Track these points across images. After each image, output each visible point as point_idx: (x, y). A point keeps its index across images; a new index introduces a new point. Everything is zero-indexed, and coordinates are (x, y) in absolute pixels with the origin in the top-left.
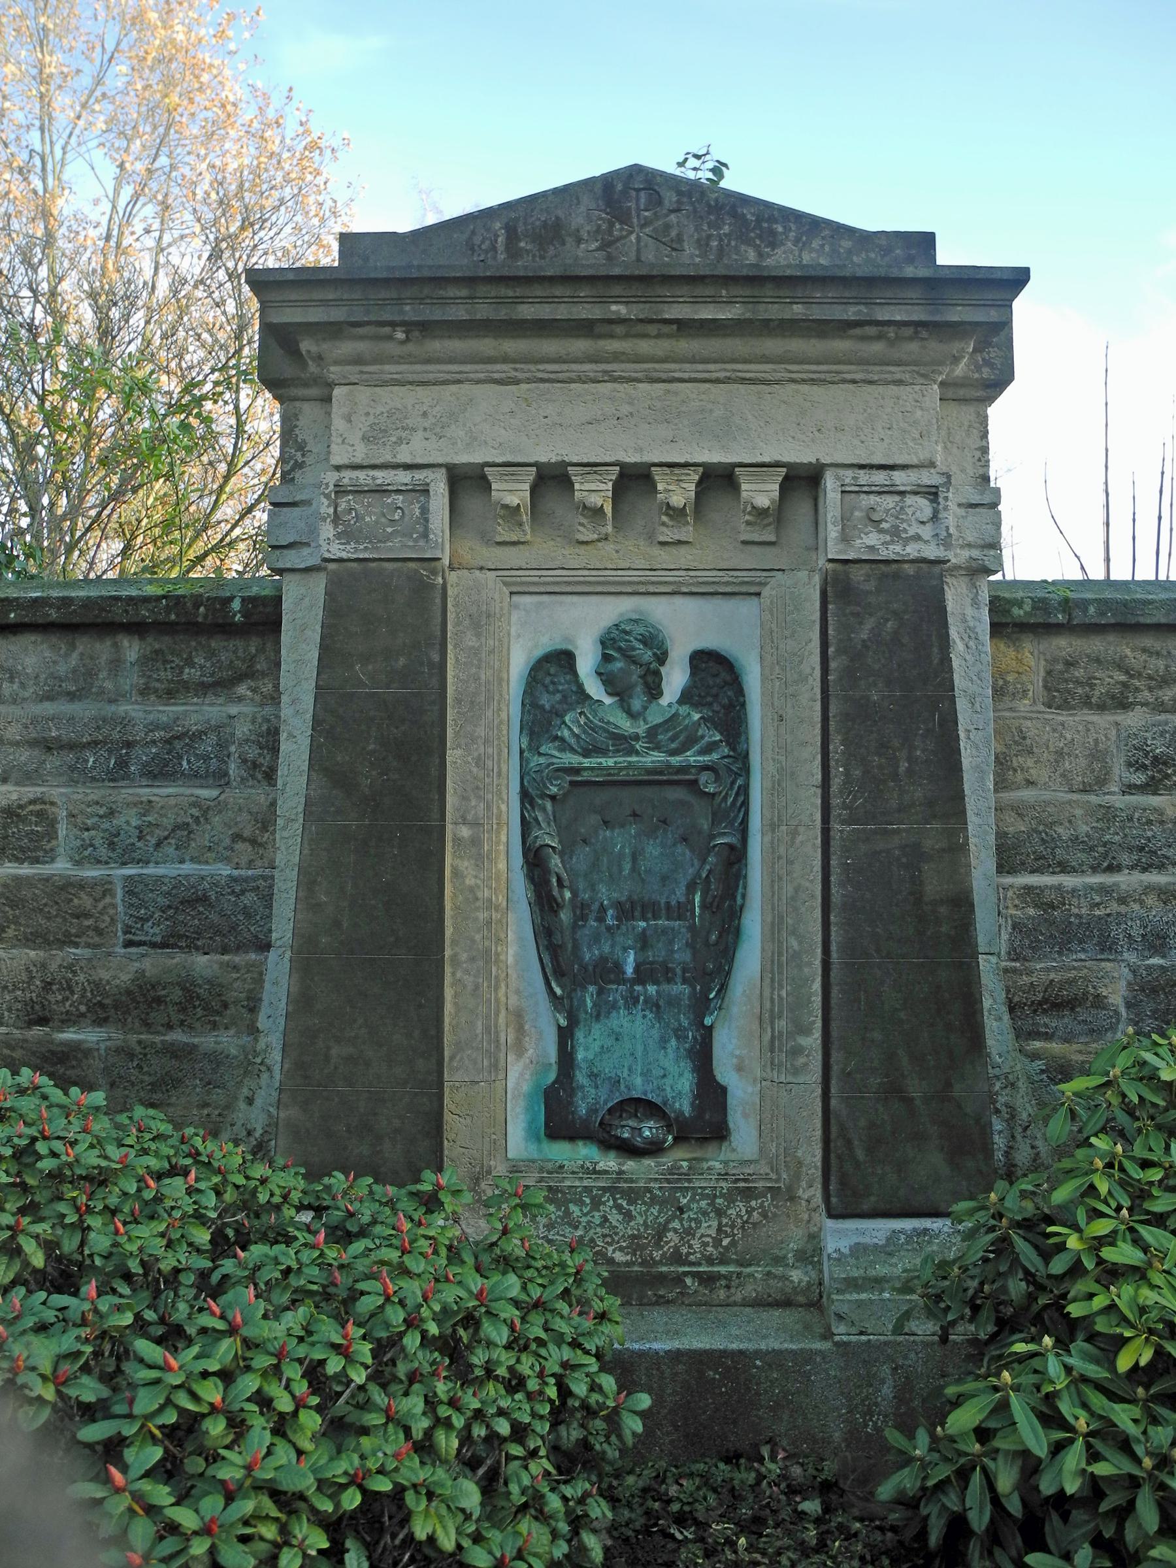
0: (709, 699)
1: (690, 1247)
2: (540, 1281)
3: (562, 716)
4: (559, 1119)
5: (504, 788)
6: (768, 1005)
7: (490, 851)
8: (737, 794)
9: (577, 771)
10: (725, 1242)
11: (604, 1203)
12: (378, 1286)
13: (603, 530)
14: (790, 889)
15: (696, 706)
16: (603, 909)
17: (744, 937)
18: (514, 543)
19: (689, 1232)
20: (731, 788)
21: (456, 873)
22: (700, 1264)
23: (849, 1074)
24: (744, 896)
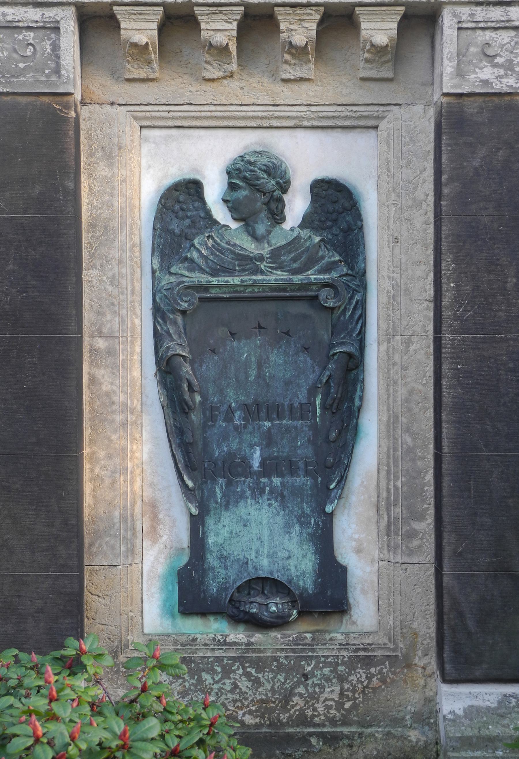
0: (329, 223)
1: (315, 709)
2: (177, 733)
3: (191, 240)
4: (192, 594)
5: (137, 305)
6: (384, 495)
7: (125, 361)
8: (355, 308)
9: (206, 288)
10: (347, 705)
11: (234, 672)
12: (29, 730)
13: (229, 68)
14: (404, 391)
15: (315, 229)
16: (231, 411)
17: (362, 434)
18: (143, 80)
19: (314, 697)
20: (350, 303)
21: (93, 380)
22: (324, 726)
23: (460, 554)
24: (361, 399)
